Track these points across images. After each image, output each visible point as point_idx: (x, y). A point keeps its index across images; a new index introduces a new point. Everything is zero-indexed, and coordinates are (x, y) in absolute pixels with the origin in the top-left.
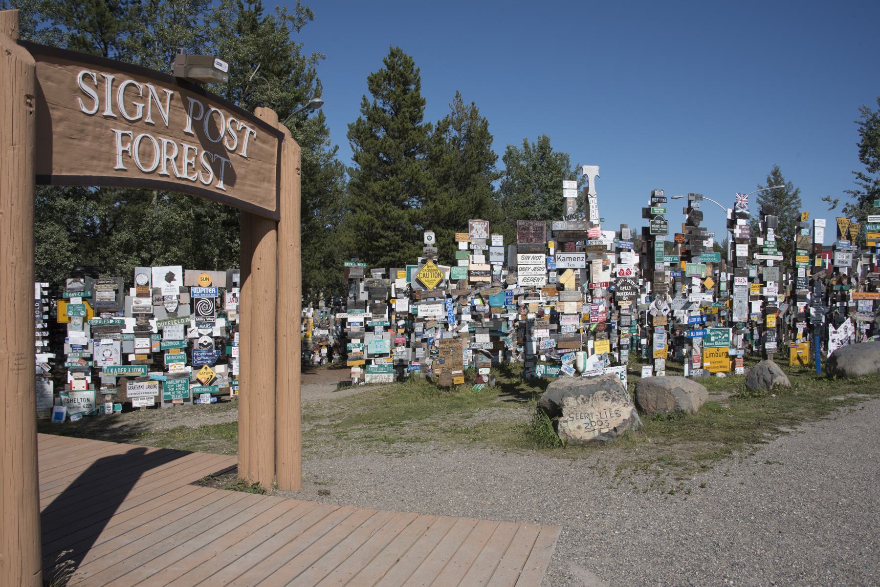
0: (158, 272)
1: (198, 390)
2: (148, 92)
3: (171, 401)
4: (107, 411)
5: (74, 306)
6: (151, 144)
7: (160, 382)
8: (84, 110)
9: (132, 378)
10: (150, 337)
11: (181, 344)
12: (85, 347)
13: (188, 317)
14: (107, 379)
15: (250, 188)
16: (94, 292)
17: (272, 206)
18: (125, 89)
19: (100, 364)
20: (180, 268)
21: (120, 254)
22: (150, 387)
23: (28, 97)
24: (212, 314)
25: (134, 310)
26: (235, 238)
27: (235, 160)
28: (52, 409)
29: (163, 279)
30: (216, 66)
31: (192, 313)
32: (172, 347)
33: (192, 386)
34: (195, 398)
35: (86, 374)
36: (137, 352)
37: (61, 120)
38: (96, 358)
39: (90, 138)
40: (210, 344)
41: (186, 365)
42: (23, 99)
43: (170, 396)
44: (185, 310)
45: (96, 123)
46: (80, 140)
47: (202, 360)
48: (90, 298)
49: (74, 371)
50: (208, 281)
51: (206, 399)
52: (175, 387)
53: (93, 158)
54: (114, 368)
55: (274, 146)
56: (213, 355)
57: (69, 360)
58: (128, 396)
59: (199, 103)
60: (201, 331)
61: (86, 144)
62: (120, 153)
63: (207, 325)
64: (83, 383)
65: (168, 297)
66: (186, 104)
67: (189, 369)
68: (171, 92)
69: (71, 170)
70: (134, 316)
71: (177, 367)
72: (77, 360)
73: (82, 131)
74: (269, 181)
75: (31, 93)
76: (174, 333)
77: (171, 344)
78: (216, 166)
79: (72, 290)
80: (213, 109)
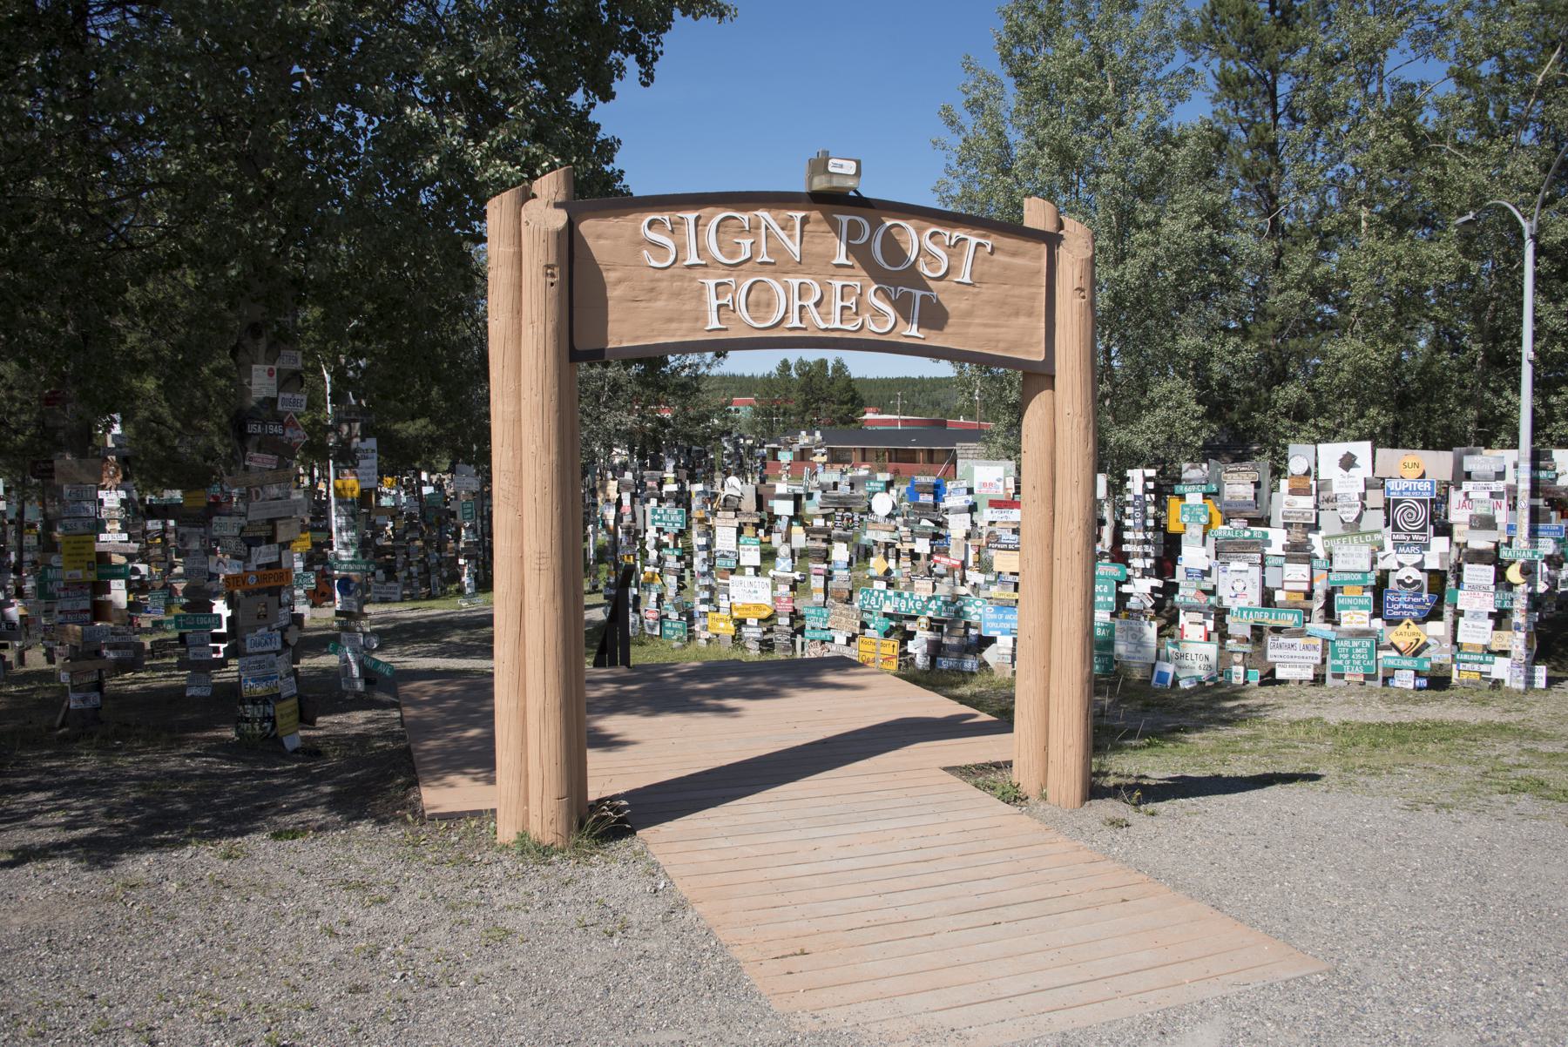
0: (1331, 452)
1: (1391, 663)
2: (759, 223)
3: (1342, 676)
4: (1234, 681)
5: (1191, 507)
6: (769, 289)
7: (1325, 641)
8: (654, 263)
9: (1277, 630)
10: (1310, 563)
11: (1365, 579)
12: (1206, 573)
13: (1379, 532)
14: (1238, 627)
15: (981, 330)
16: (1220, 483)
17: (1039, 353)
18: (718, 226)
19: (1226, 603)
20: (1368, 444)
21: (1287, 422)
22: (1306, 647)
23: (548, 267)
24: (1424, 529)
25: (1284, 517)
26: (1503, 389)
27: (945, 290)
28: (1153, 665)
29: (1341, 467)
30: (831, 169)
31: (1387, 525)
32: (1349, 582)
33: (1381, 654)
34: (1385, 680)
35: (1206, 616)
36: (1287, 586)
37: (619, 281)
38: (1220, 592)
39: (664, 297)
40: (1417, 582)
41: (1374, 615)
42: (541, 271)
43: (1341, 667)
44: (1375, 520)
45: (673, 276)
46: (649, 300)
47: (1402, 609)
48: (1217, 494)
49: (1189, 609)
50: (1416, 469)
51: (1405, 680)
52: (1350, 653)
53: (670, 320)
54: (1249, 610)
55: (1039, 257)
56: (1422, 603)
57: (1181, 591)
58: (1270, 659)
59: (859, 219)
60: (1401, 558)
61: (660, 304)
62: (715, 308)
63: (1413, 549)
64: (1201, 630)
65: (1344, 495)
66: (835, 226)
67: (1378, 623)
68: (800, 214)
69: (637, 338)
70: (1287, 526)
71: (1355, 617)
72: (1192, 593)
73: (652, 290)
74: (1030, 314)
75: (552, 261)
76: (1353, 558)
77: (1347, 577)
78: (903, 307)
79: (1189, 482)
80: (888, 223)
